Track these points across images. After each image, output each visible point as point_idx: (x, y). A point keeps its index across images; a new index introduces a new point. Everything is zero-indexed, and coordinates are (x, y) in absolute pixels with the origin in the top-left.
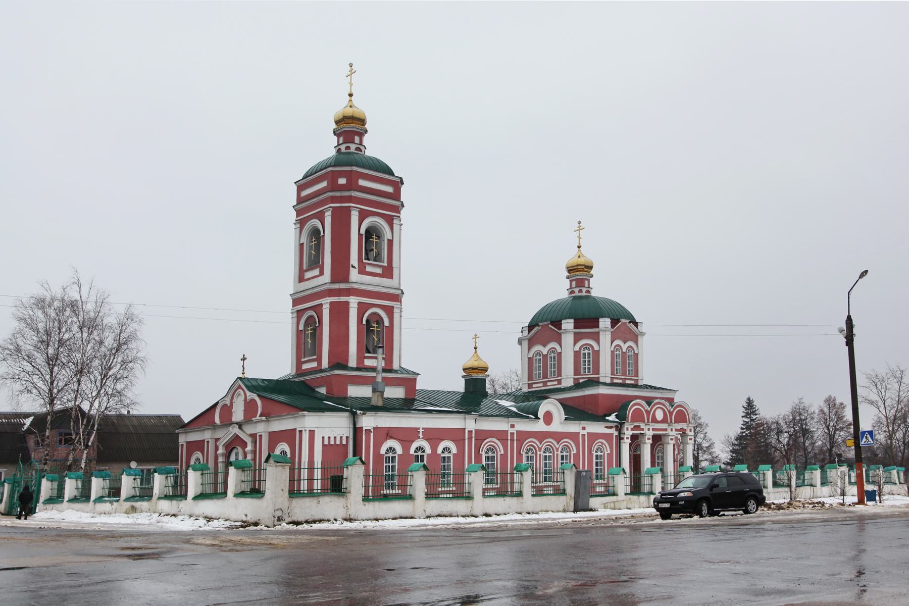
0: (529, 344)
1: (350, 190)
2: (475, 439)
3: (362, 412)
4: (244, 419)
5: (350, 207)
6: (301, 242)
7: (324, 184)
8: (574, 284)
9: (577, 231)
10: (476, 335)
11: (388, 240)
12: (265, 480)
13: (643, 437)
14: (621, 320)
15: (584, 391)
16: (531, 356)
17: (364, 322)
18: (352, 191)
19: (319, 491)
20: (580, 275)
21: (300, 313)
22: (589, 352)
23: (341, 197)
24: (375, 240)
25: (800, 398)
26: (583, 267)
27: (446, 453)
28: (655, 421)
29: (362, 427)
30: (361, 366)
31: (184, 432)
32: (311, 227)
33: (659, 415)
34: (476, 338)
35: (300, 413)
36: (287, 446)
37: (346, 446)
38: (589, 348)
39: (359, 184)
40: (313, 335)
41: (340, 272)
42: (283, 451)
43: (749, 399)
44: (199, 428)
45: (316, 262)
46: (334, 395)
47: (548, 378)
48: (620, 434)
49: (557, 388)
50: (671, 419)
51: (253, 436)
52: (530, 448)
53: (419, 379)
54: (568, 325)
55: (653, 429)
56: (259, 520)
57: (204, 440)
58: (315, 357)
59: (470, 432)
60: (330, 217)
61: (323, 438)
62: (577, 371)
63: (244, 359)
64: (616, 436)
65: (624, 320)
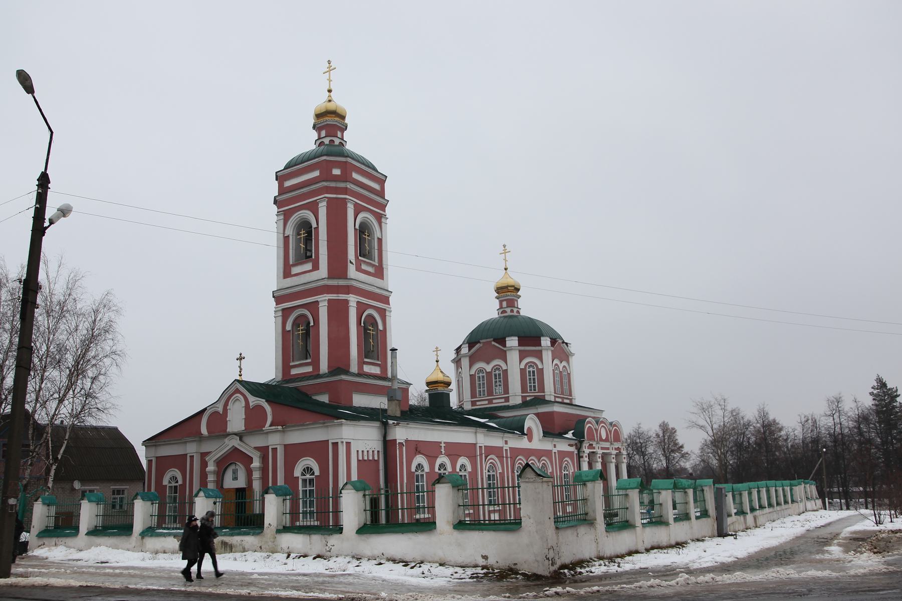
0: (470, 361)
1: (347, 182)
3: (396, 422)
4: (245, 429)
5: (346, 199)
7: (316, 173)
8: (505, 304)
9: (502, 254)
10: (437, 348)
12: (554, 503)
13: (595, 456)
15: (537, 408)
16: (473, 372)
17: (362, 325)
18: (348, 183)
20: (510, 296)
21: (286, 313)
22: (534, 369)
23: (336, 188)
24: (367, 237)
25: (639, 423)
26: (513, 288)
27: (442, 470)
28: (601, 440)
29: (396, 440)
30: (361, 372)
31: (153, 445)
32: (299, 219)
34: (437, 351)
35: (336, 421)
37: (377, 462)
38: (533, 366)
40: (307, 334)
41: (338, 268)
44: (181, 440)
45: (307, 254)
46: (341, 404)
47: (494, 396)
48: (579, 452)
49: (505, 406)
54: (512, 342)
55: (601, 447)
56: (515, 564)
57: (187, 454)
58: (309, 361)
59: (480, 447)
60: (325, 208)
61: (358, 451)
62: (524, 389)
63: (241, 358)
64: (576, 454)
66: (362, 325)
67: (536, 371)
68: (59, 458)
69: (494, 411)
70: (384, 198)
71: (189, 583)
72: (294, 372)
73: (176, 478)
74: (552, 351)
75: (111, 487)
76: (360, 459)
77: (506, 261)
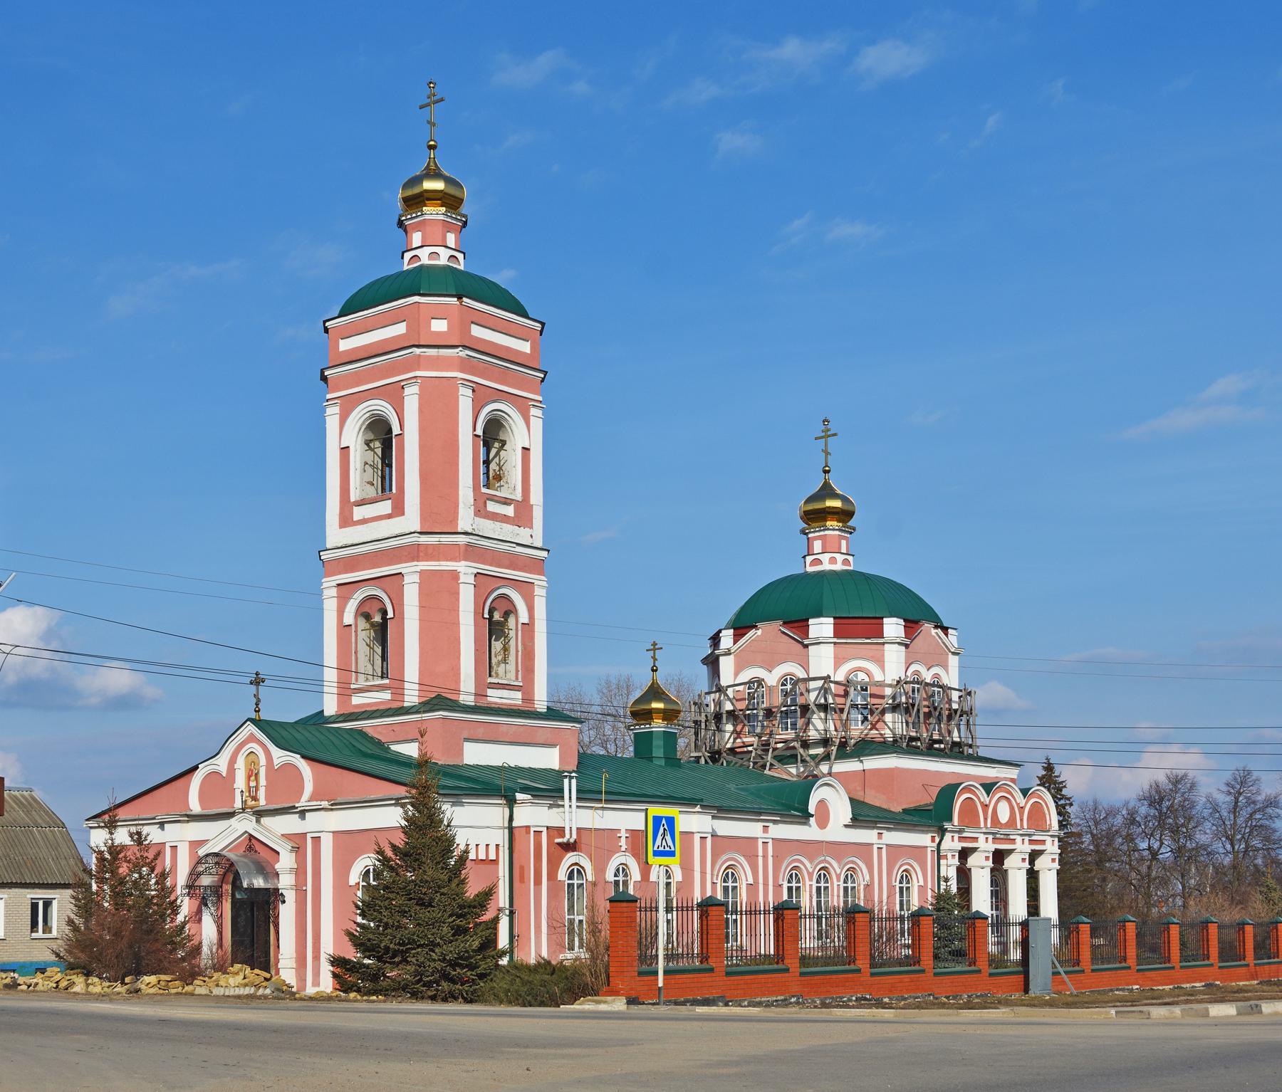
10: (655, 644)
17: (486, 616)
32: (368, 415)
34: (654, 650)
39: (405, 332)
51: (298, 842)
68: (109, 857)
71: (228, 869)
72: (357, 700)
77: (827, 453)
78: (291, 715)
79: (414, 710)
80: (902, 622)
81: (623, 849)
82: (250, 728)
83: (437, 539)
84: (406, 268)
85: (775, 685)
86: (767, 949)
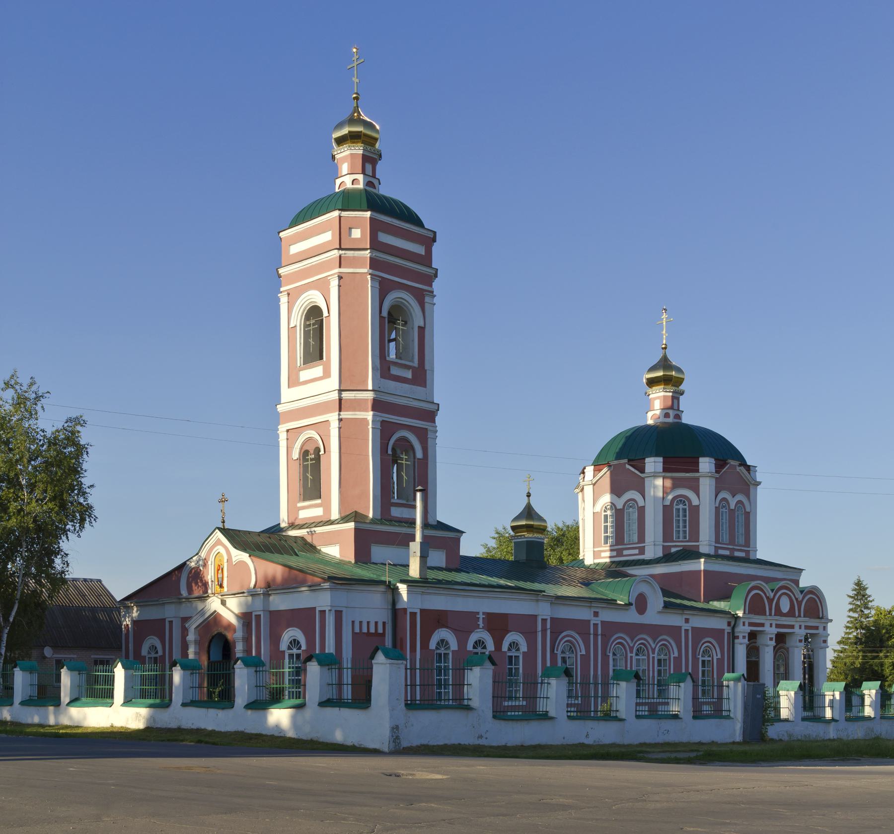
2: (551, 632)
6: (292, 325)
11: (419, 327)
14: (729, 461)
17: (390, 452)
19: (350, 701)
22: (685, 507)
28: (778, 612)
33: (785, 606)
36: (300, 632)
38: (684, 502)
42: (295, 640)
43: (859, 584)
50: (770, 609)
52: (641, 647)
53: (463, 540)
61: (353, 622)
62: (667, 535)
63: (223, 501)
64: (728, 633)
65: (733, 462)
66: (390, 452)
67: (687, 509)
69: (623, 566)
70: (429, 265)
73: (156, 648)
74: (716, 478)
75: (92, 656)
76: (356, 632)
78: (258, 526)
79: (336, 522)
80: (713, 460)
81: (481, 627)
82: (219, 535)
83: (353, 395)
84: (337, 190)
85: (622, 508)
86: (726, 707)
